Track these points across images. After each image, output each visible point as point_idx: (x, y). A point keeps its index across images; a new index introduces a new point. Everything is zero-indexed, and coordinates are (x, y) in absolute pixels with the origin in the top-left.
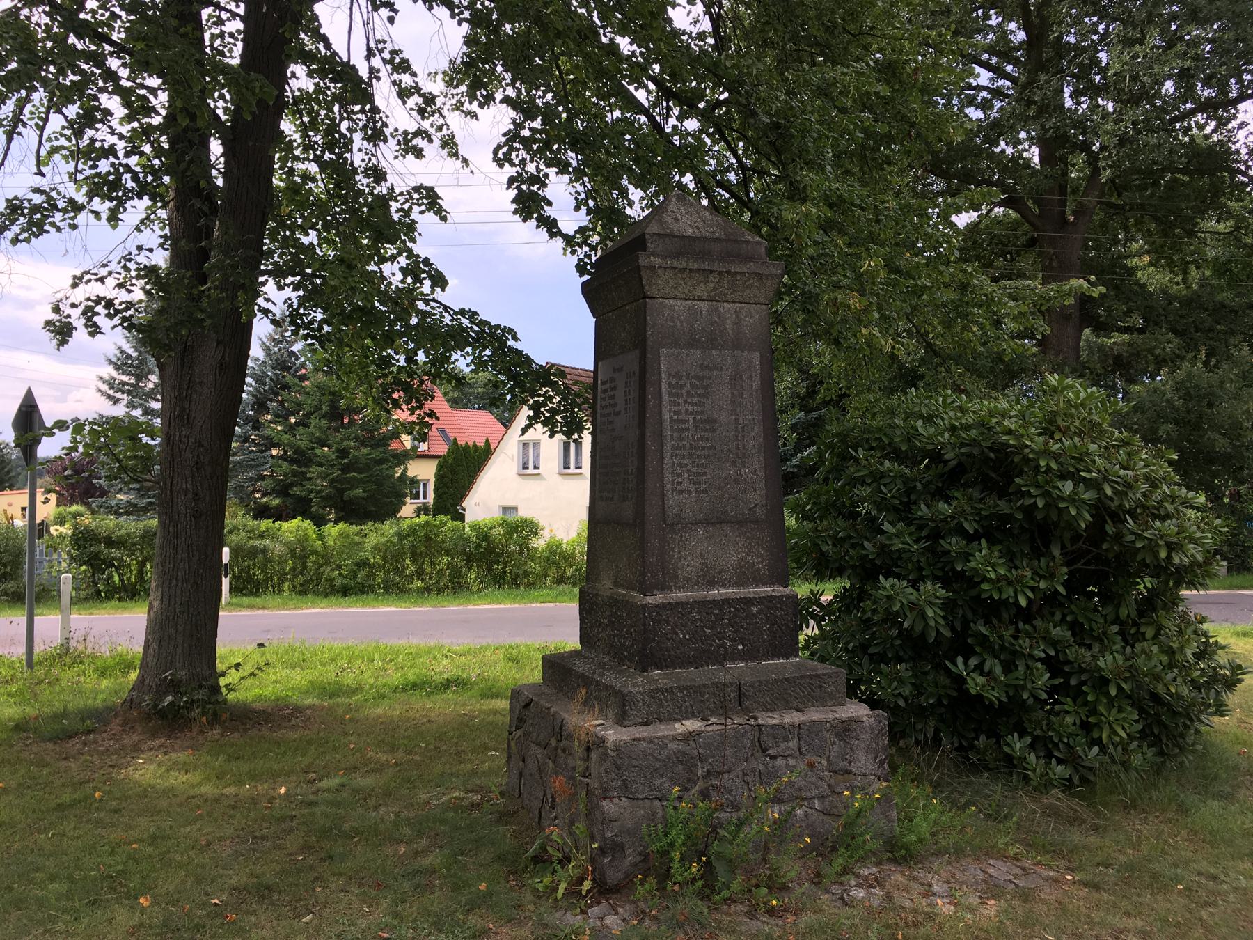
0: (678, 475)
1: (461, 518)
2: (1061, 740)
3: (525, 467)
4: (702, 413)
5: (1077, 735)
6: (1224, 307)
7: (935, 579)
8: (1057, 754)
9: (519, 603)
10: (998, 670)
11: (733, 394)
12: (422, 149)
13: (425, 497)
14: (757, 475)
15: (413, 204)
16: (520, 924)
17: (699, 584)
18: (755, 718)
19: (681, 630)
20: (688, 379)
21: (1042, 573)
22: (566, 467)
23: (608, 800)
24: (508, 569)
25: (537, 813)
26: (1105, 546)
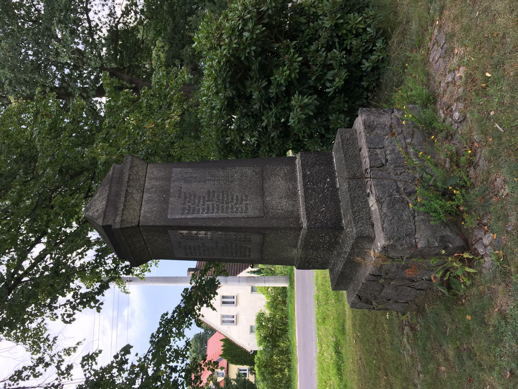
0: (237, 209)
1: (255, 352)
2: (364, 46)
3: (233, 322)
4: (204, 197)
5: (362, 38)
6: (173, 29)
7: (289, 100)
8: (371, 47)
9: (295, 322)
10: (332, 72)
11: (194, 182)
12: (68, 366)
13: (246, 370)
14: (238, 170)
15: (91, 369)
16: (494, 292)
17: (296, 201)
18: (366, 170)
19: (320, 209)
20: (185, 204)
21: (286, 51)
22: (233, 303)
23: (417, 244)
24: (279, 328)
25: (418, 292)
26: (274, 23)
